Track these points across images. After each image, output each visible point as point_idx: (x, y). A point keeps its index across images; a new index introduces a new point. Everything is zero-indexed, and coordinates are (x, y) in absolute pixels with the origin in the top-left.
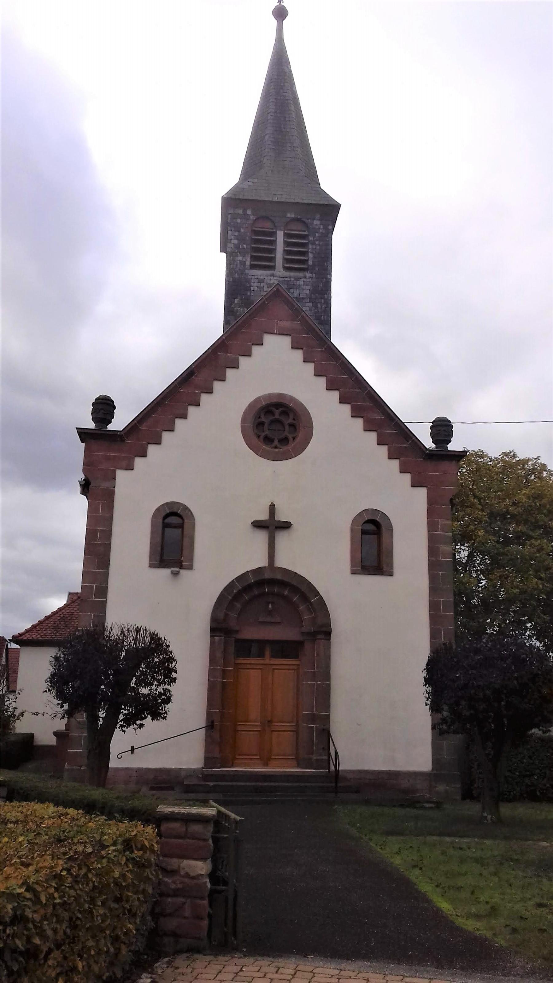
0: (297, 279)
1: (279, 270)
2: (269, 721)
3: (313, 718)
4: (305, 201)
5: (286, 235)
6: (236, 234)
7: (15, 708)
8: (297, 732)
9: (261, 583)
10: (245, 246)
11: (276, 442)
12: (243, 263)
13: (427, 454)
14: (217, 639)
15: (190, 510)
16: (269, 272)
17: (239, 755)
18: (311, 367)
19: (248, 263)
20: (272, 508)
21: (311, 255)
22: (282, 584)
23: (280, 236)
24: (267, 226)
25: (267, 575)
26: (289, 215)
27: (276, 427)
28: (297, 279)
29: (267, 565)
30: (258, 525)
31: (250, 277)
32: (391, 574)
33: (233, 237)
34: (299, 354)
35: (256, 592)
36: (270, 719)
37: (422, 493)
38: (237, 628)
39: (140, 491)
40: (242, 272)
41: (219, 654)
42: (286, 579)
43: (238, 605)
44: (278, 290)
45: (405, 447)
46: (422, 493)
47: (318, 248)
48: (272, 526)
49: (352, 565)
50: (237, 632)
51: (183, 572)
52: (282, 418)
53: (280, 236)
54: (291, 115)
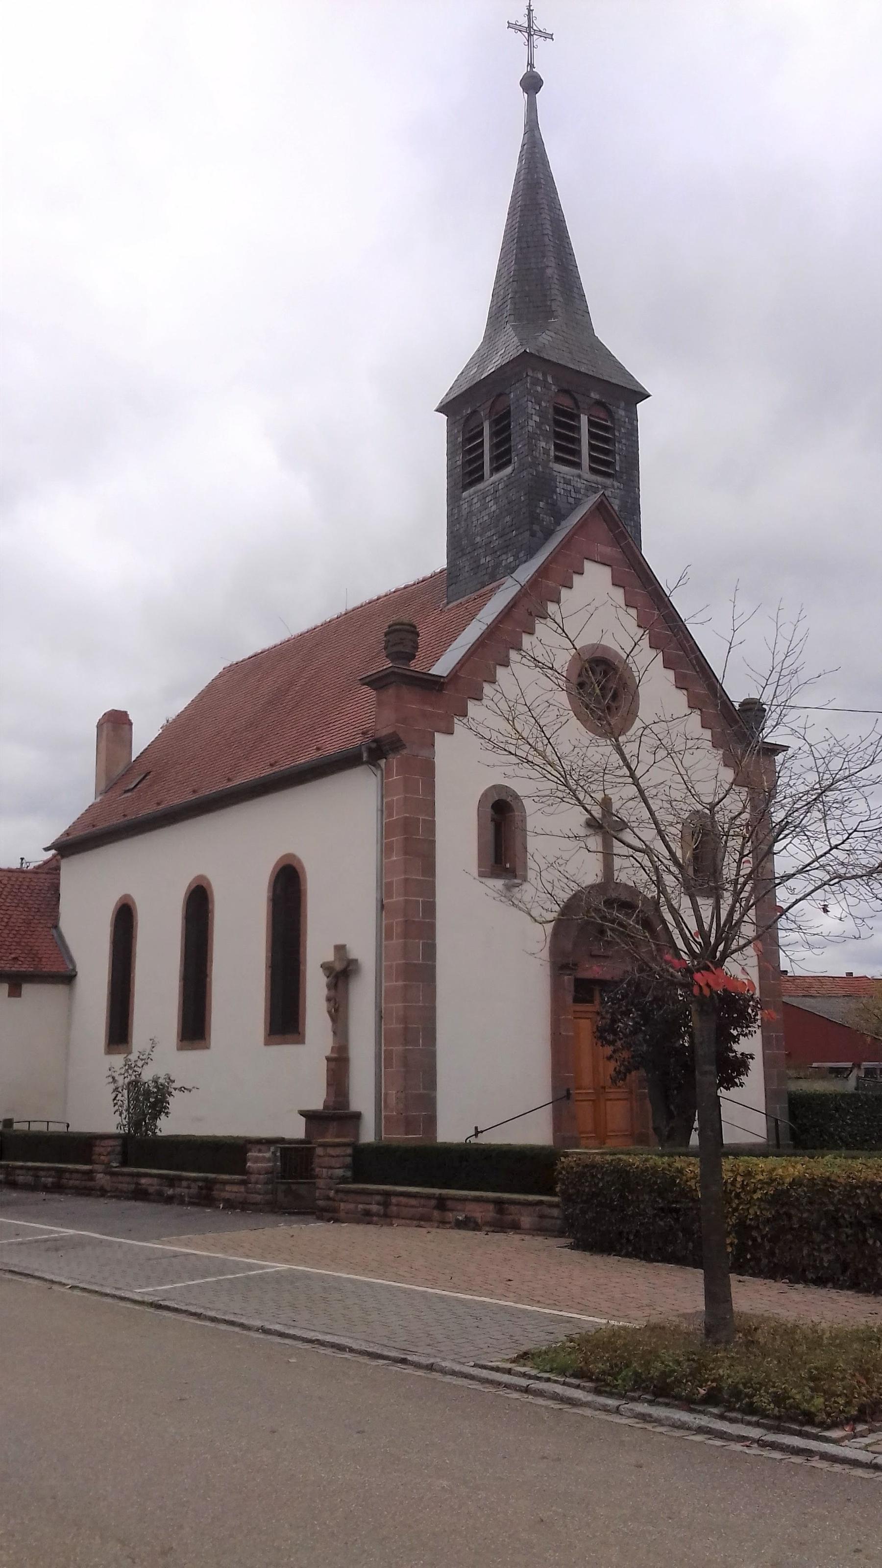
4: (613, 381)
5: (591, 423)
7: (609, 1058)
12: (546, 452)
23: (584, 419)
31: (555, 474)
33: (534, 411)
34: (619, 595)
53: (584, 419)
54: (544, 227)
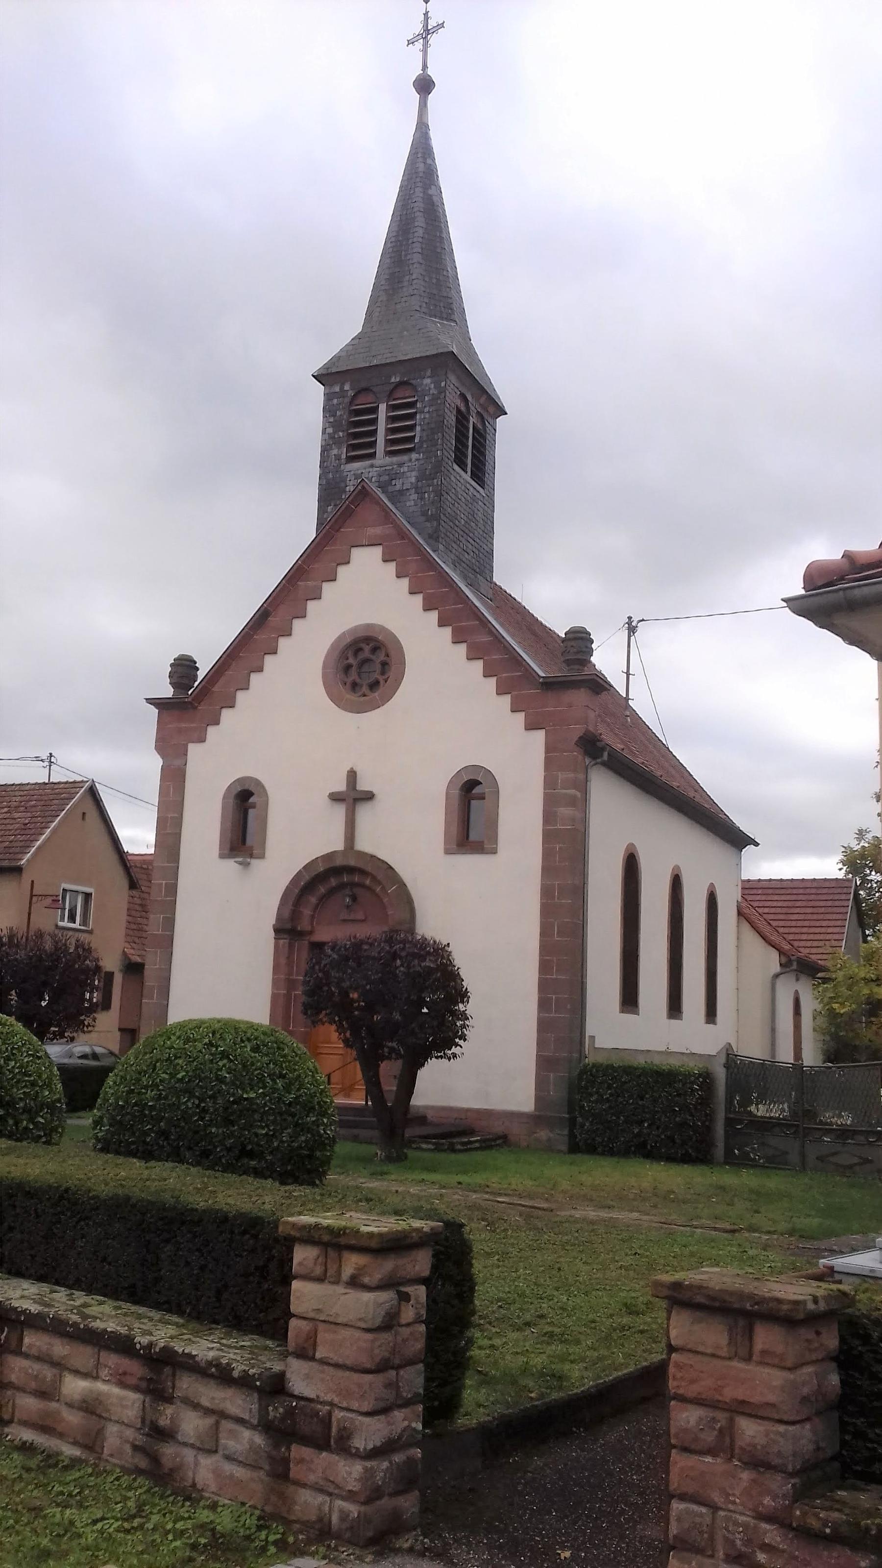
0: (401, 465)
1: (381, 459)
6: (332, 420)
10: (341, 434)
11: (365, 689)
13: (542, 684)
14: (281, 942)
16: (368, 463)
18: (405, 582)
19: (344, 456)
20: (352, 775)
21: (418, 428)
24: (364, 402)
26: (393, 380)
27: (365, 668)
28: (401, 465)
30: (336, 798)
32: (494, 852)
35: (333, 882)
37: (539, 737)
39: (214, 764)
40: (337, 470)
41: (283, 961)
43: (313, 900)
44: (363, 487)
45: (520, 676)
46: (539, 737)
47: (427, 416)
49: (446, 842)
50: (311, 933)
51: (254, 862)
52: (361, 656)
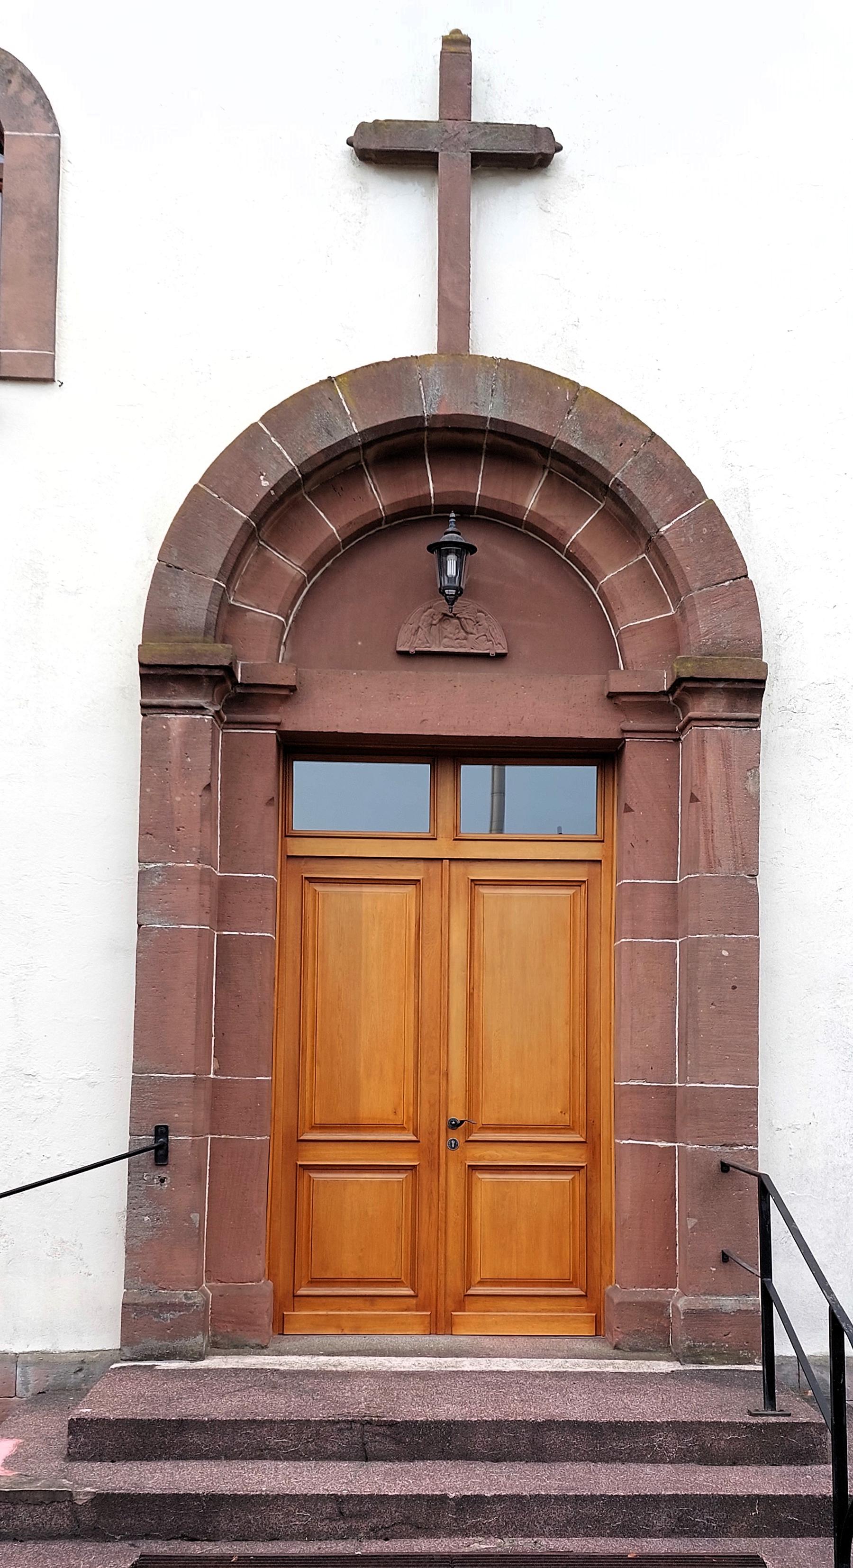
2: (454, 1125)
3: (668, 1110)
8: (588, 1174)
9: (400, 445)
14: (176, 722)
15: (30, 81)
17: (314, 1282)
22: (513, 449)
25: (434, 401)
29: (431, 348)
36: (457, 1113)
38: (284, 676)
42: (528, 418)
43: (291, 566)
48: (458, 154)
50: (288, 693)
